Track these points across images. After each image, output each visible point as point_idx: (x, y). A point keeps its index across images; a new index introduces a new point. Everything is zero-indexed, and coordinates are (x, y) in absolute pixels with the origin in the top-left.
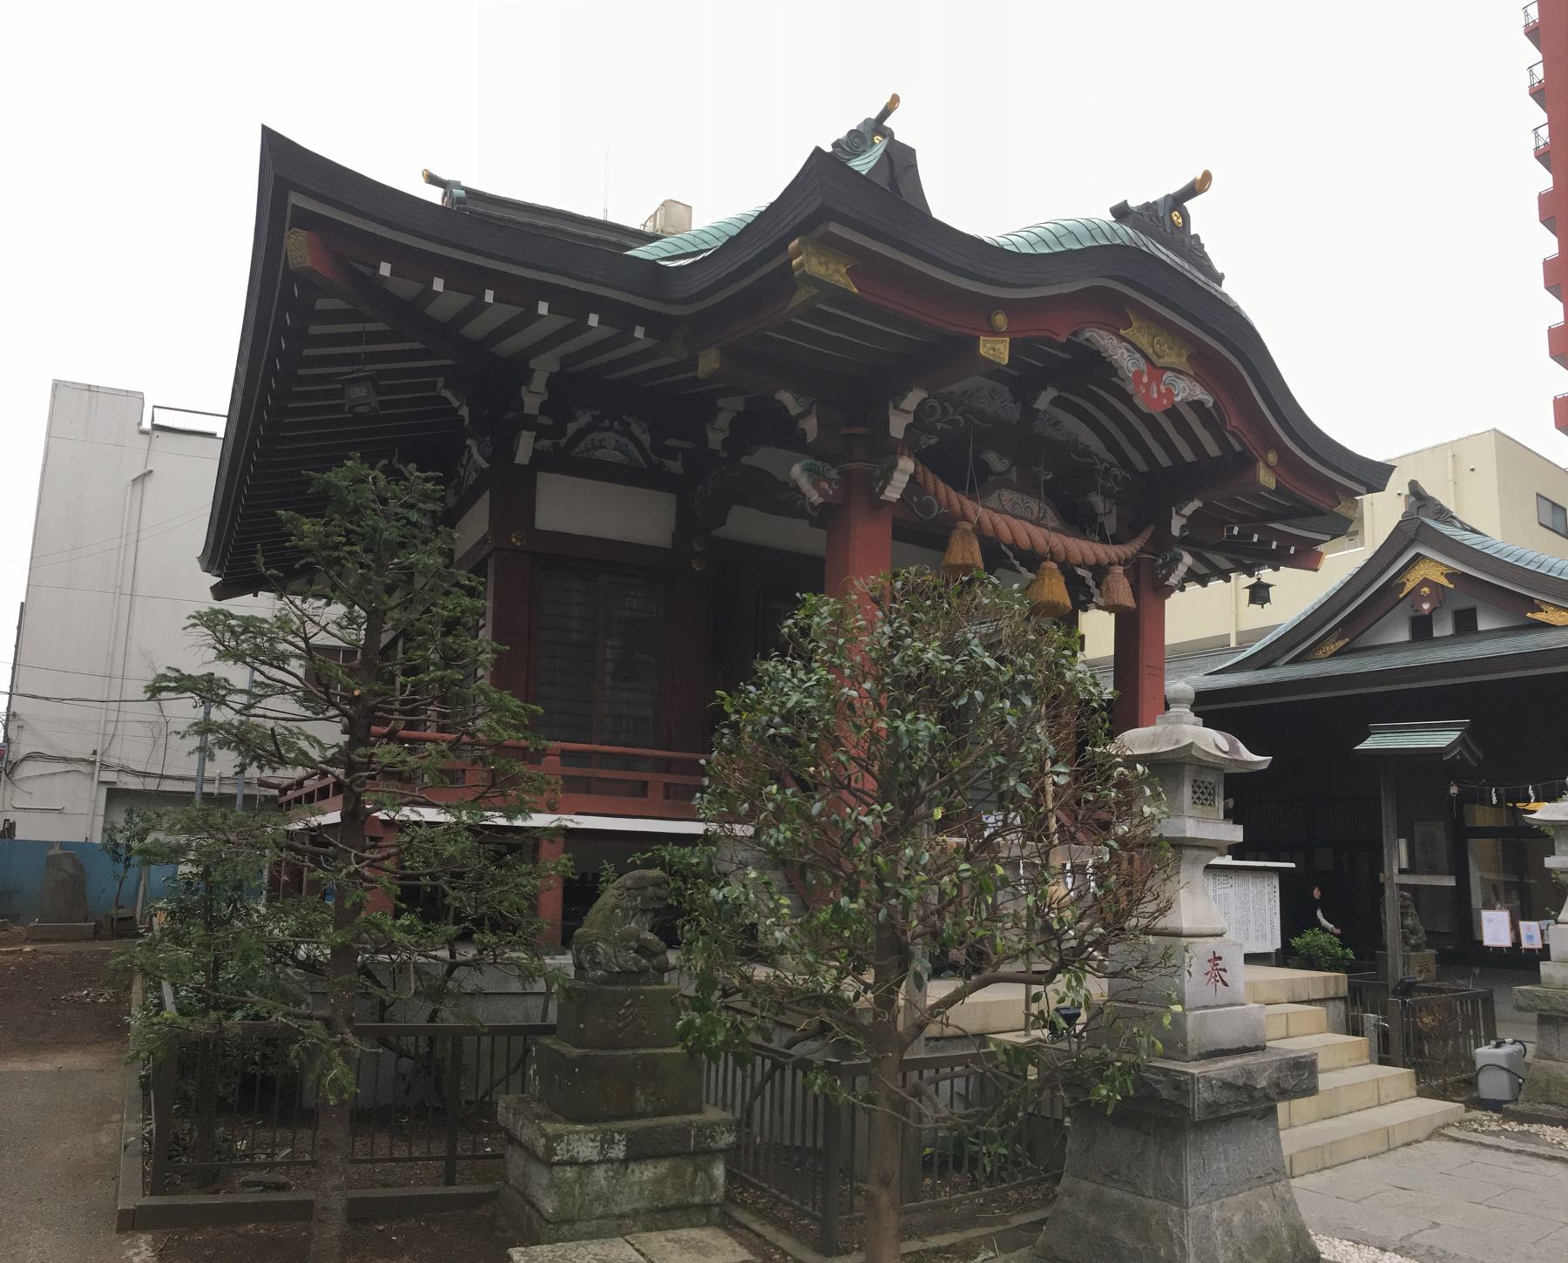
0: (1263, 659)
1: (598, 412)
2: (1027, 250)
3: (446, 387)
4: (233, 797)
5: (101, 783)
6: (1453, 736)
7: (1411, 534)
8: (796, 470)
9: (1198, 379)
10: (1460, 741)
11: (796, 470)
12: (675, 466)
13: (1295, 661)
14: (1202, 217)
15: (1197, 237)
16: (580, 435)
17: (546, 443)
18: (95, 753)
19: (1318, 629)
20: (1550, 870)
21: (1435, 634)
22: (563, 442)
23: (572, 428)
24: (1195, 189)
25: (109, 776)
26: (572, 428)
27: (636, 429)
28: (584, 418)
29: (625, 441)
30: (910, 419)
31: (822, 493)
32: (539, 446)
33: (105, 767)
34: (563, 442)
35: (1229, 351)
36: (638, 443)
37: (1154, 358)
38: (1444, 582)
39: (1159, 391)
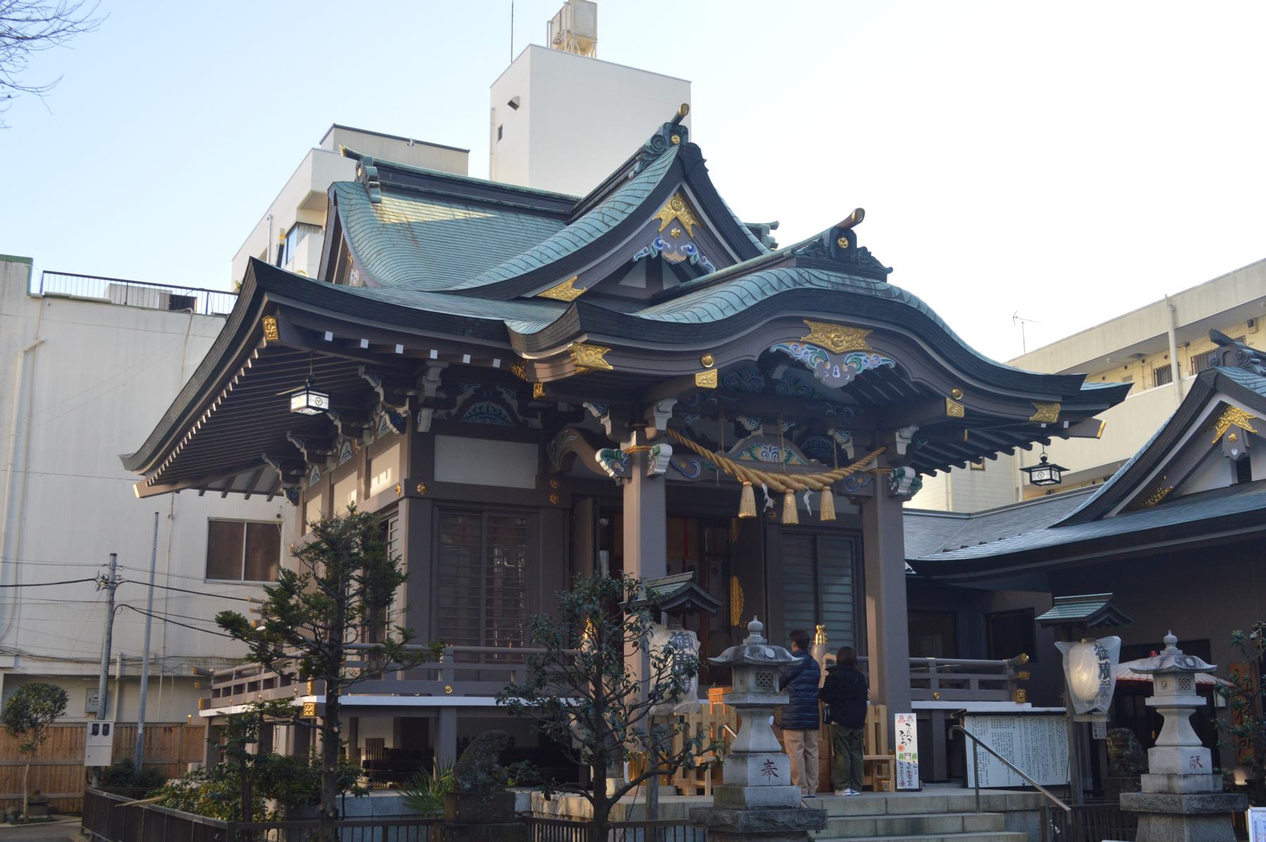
0: (1093, 513)
4: (894, 753)
6: (1099, 606)
8: (598, 457)
11: (598, 457)
12: (536, 423)
13: (1127, 510)
14: (864, 236)
15: (864, 249)
17: (442, 413)
20: (1150, 707)
21: (1255, 478)
22: (453, 411)
23: (460, 400)
24: (860, 214)
26: (460, 400)
29: (498, 407)
30: (670, 415)
34: (453, 411)
36: (508, 407)
37: (832, 348)
39: (841, 371)
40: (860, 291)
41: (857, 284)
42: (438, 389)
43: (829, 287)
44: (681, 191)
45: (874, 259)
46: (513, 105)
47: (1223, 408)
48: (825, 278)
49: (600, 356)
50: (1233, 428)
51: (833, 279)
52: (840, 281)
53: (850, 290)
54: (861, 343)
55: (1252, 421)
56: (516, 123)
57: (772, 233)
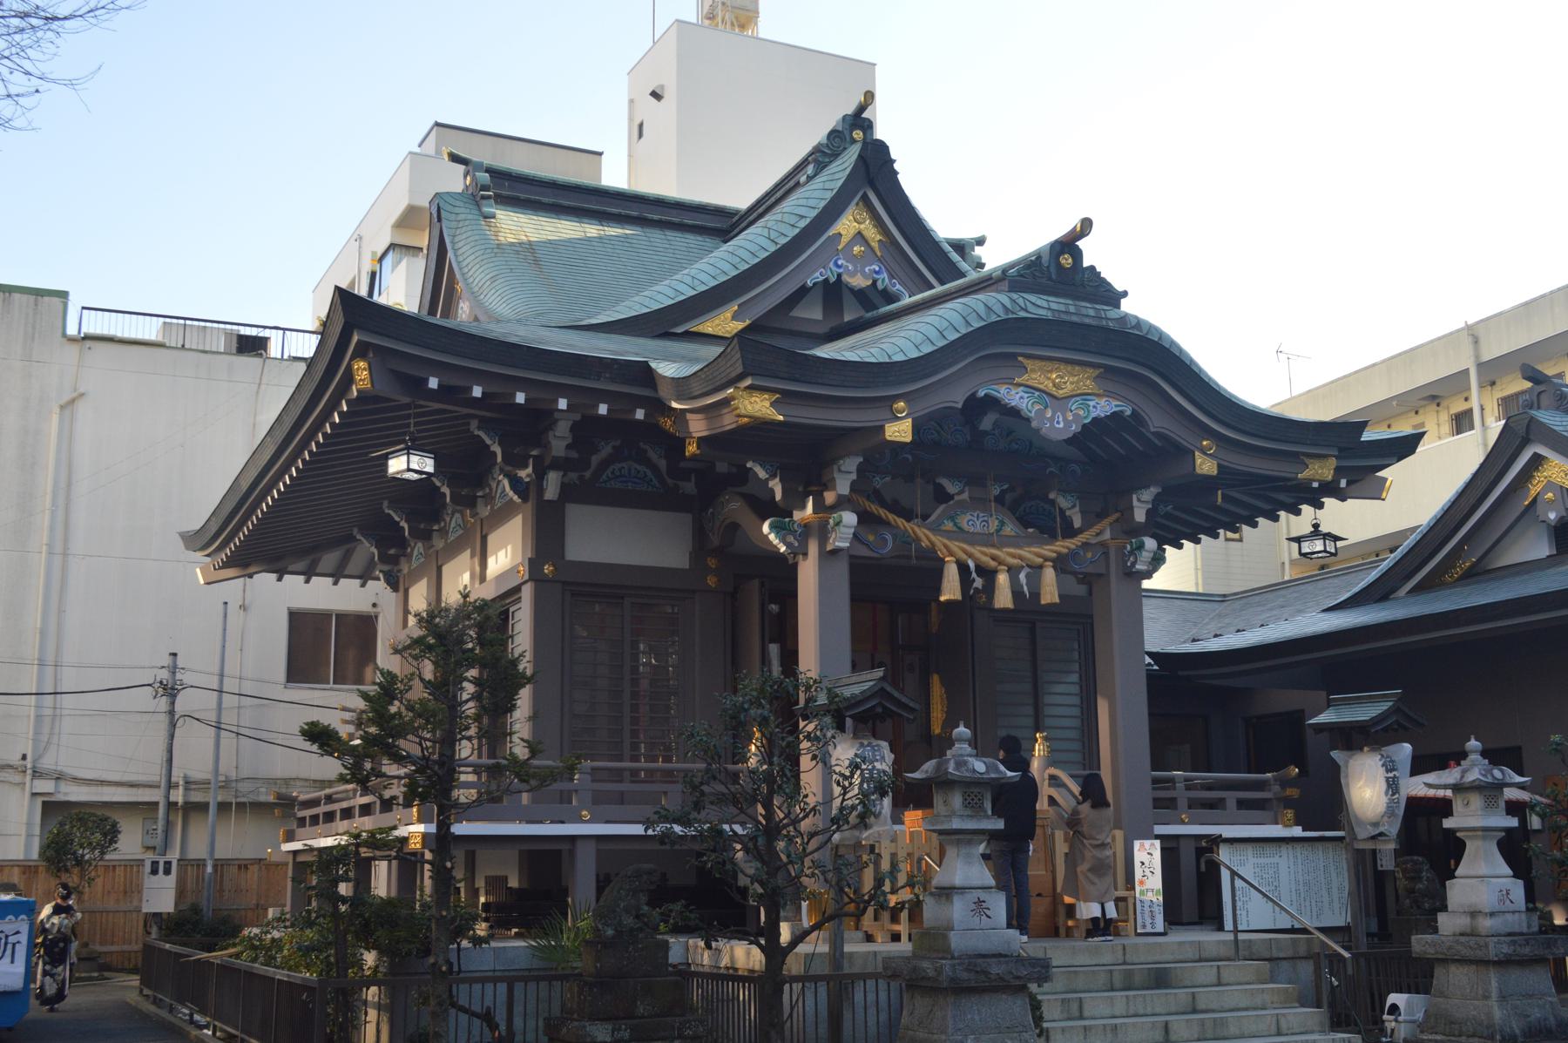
1: (618, 443)
2: (914, 354)
3: (479, 428)
5: (34, 794)
8: (766, 528)
9: (1109, 394)
11: (766, 528)
12: (689, 487)
14: (1092, 252)
15: (1092, 268)
17: (573, 476)
18: (24, 757)
20: (1449, 830)
22: (588, 474)
25: (45, 786)
30: (854, 476)
31: (788, 545)
32: (566, 480)
33: (37, 774)
34: (588, 474)
36: (654, 468)
37: (1054, 391)
39: (1065, 419)
40: (1087, 321)
41: (1084, 311)
42: (568, 447)
43: (1049, 315)
44: (865, 199)
45: (1104, 281)
47: (1537, 461)
48: (1045, 304)
49: (767, 404)
51: (1054, 306)
52: (1062, 308)
53: (1075, 319)
54: (1088, 385)
56: (660, 117)
57: (978, 251)
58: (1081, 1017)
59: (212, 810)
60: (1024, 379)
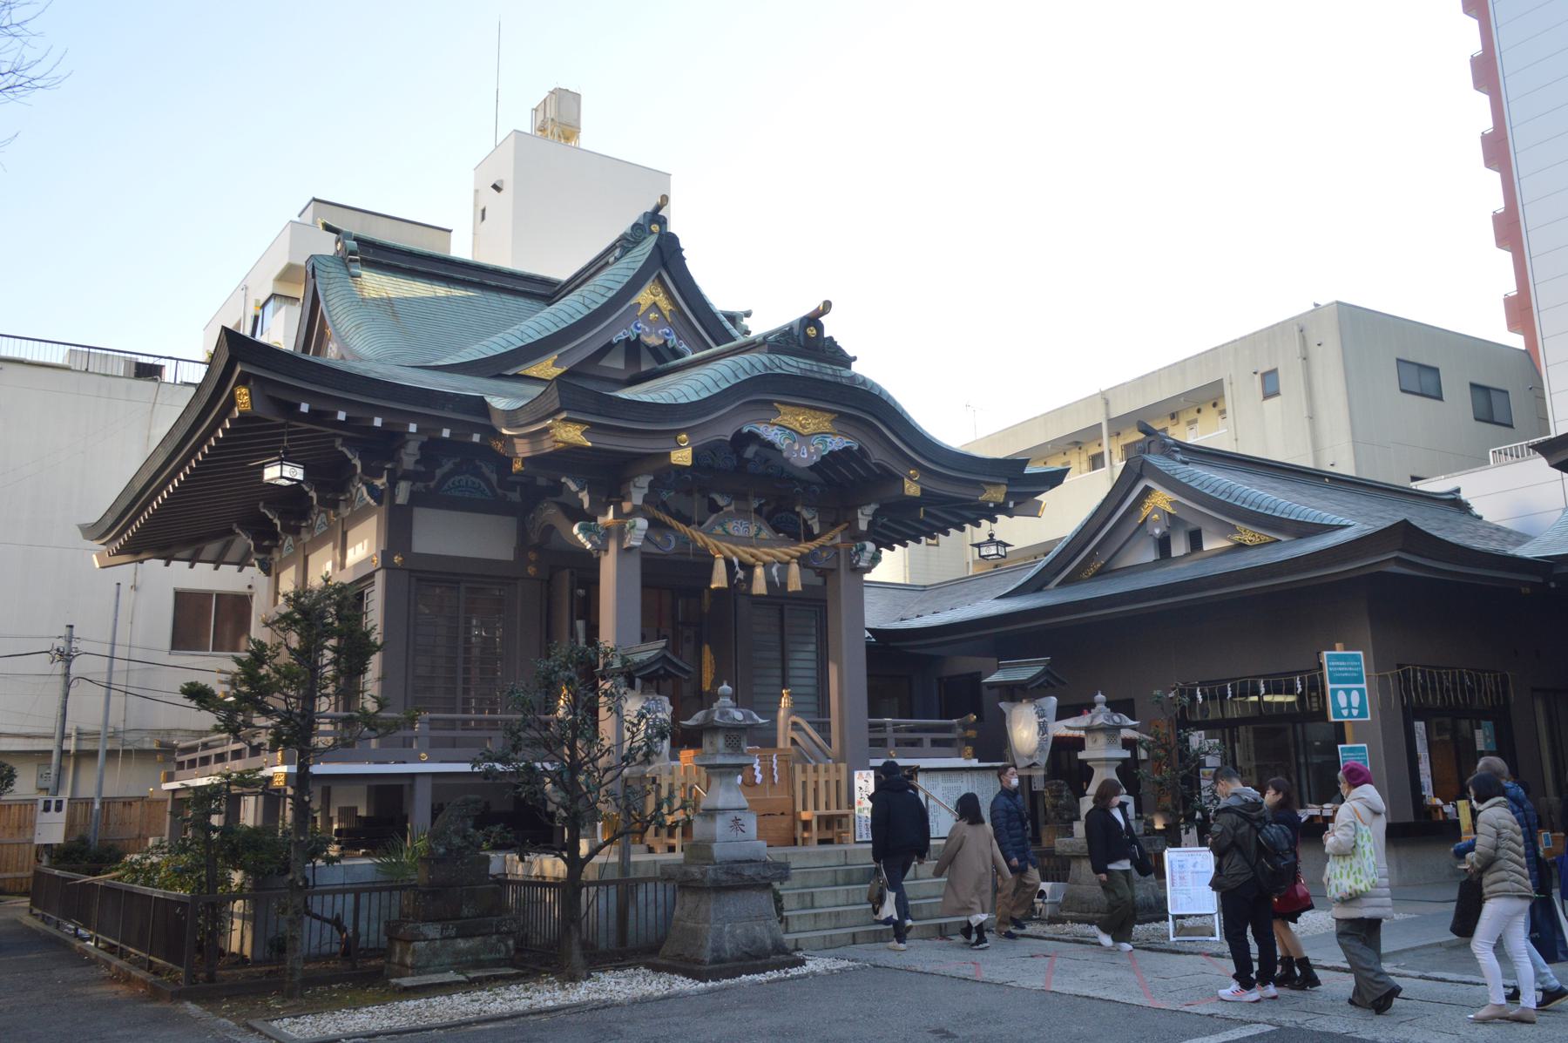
0: (1034, 585)
7: (1137, 470)
8: (575, 530)
9: (842, 433)
10: (1045, 672)
11: (575, 530)
12: (515, 496)
14: (832, 327)
15: (831, 338)
16: (446, 477)
17: (420, 485)
19: (1073, 559)
22: (432, 484)
23: (439, 473)
27: (486, 470)
28: (448, 466)
30: (646, 491)
34: (432, 484)
35: (870, 409)
36: (487, 481)
37: (800, 430)
38: (1170, 510)
42: (417, 462)
43: (798, 372)
46: (495, 187)
47: (1147, 491)
50: (1156, 509)
55: (1172, 503)
56: (501, 206)
58: (813, 907)
59: (101, 756)
60: (778, 420)
